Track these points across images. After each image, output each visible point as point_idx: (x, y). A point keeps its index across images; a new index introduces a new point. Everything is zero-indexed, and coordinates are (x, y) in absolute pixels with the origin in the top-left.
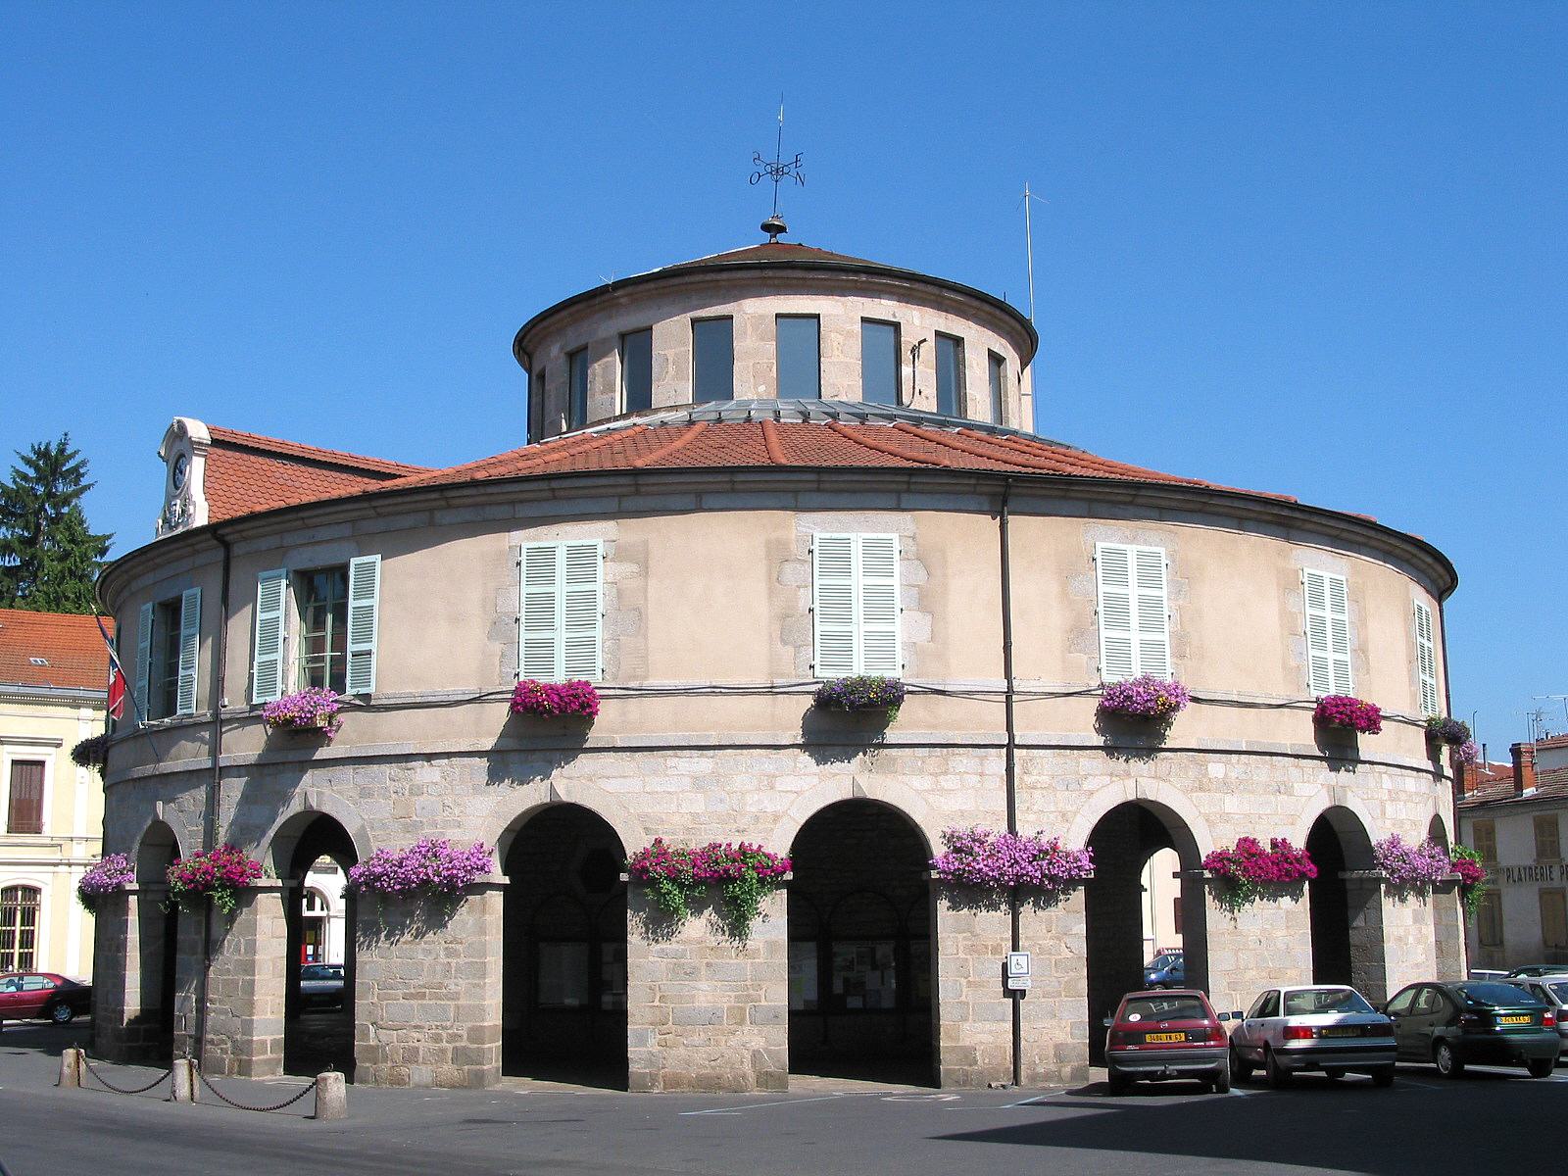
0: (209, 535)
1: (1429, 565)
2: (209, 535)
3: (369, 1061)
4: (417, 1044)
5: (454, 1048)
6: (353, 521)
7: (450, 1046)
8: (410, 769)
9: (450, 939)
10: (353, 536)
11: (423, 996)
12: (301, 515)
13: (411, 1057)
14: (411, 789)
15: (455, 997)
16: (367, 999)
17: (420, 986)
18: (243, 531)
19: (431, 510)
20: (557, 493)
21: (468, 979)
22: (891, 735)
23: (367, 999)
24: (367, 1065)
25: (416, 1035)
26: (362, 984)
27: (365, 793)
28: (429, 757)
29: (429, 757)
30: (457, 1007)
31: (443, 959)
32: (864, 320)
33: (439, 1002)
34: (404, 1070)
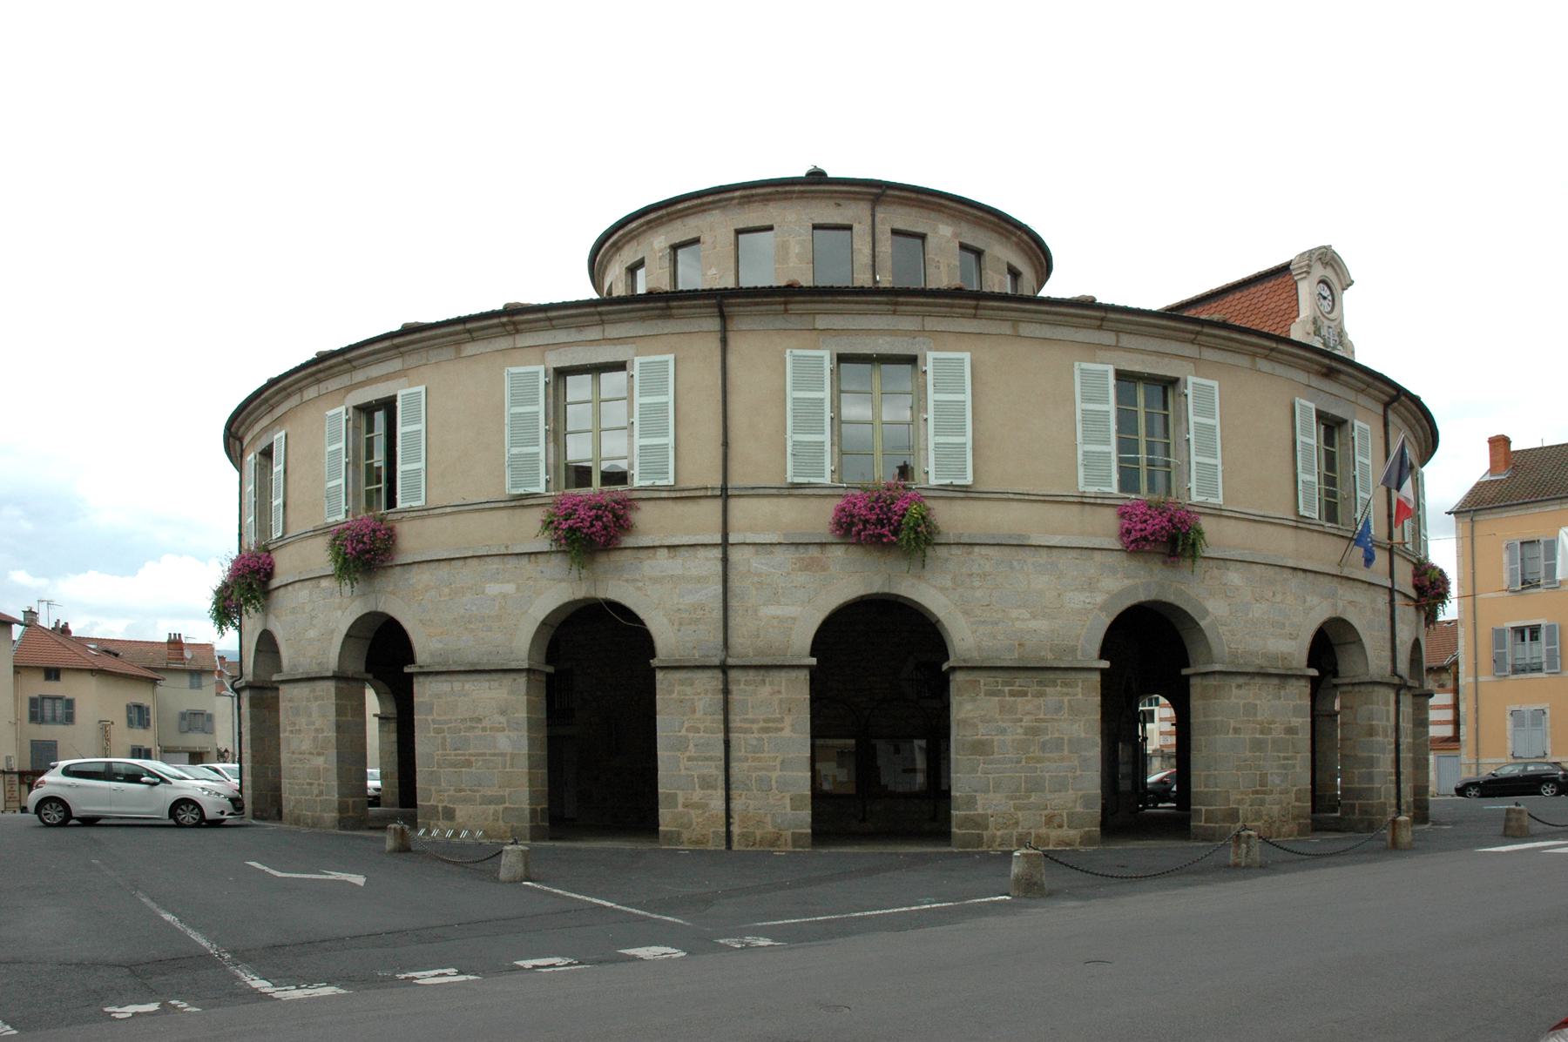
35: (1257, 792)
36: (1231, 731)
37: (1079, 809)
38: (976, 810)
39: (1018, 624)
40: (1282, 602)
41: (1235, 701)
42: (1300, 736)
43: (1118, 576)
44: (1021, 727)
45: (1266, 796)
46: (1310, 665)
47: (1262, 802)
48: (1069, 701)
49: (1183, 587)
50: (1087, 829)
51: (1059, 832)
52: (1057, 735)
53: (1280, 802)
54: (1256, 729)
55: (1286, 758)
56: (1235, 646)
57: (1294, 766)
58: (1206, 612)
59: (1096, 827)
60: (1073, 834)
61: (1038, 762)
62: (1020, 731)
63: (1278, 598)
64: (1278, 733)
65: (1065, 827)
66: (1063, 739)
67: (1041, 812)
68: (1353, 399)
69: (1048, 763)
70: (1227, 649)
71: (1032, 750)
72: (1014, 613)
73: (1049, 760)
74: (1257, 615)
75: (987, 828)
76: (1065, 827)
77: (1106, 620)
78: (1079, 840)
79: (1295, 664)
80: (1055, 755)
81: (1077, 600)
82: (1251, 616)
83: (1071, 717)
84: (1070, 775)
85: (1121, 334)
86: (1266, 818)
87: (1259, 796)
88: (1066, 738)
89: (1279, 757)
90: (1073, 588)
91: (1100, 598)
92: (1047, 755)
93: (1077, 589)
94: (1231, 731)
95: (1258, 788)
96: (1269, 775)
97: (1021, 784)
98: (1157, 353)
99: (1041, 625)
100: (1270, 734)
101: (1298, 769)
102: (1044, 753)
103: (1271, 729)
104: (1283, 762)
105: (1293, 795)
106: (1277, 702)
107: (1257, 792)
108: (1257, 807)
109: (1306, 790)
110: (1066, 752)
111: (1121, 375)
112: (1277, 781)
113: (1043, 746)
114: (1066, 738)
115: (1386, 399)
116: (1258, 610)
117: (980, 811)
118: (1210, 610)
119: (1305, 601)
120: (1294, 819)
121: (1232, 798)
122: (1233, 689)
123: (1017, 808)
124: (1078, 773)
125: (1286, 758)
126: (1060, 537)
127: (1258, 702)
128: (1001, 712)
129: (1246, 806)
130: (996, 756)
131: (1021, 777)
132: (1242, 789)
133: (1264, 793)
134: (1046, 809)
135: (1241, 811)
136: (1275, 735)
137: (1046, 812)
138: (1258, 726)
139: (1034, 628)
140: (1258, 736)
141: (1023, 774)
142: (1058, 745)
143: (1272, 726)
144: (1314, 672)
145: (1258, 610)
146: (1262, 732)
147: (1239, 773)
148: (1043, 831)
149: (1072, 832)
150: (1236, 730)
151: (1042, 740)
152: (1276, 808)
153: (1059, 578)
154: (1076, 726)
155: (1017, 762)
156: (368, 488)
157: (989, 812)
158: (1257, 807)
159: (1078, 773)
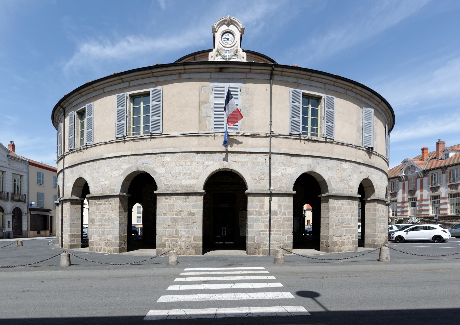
0: (70, 103)
1: (353, 87)
2: (70, 103)
3: (333, 246)
4: (344, 240)
5: (352, 241)
6: (347, 89)
7: (352, 240)
8: (341, 164)
9: (352, 212)
10: (324, 88)
11: (346, 227)
12: (80, 91)
13: (343, 244)
14: (342, 170)
15: (352, 227)
16: (332, 228)
17: (346, 224)
18: (82, 93)
19: (180, 74)
20: (124, 80)
21: (355, 222)
22: (375, 116)
23: (332, 228)
24: (333, 247)
25: (344, 238)
26: (331, 224)
27: (330, 169)
28: (346, 161)
29: (346, 161)
30: (353, 230)
31: (350, 217)
32: (13, 173)
33: (350, 229)
34: (342, 248)
35: (174, 237)
36: (163, 214)
37: (113, 241)
38: (92, 240)
39: (102, 183)
40: (190, 165)
41: (165, 204)
42: (196, 216)
43: (127, 164)
44: (100, 214)
45: (179, 239)
46: (359, 193)
47: (177, 241)
48: (111, 206)
49: (147, 165)
50: (115, 247)
51: (109, 248)
52: (108, 217)
53: (185, 242)
54: (174, 214)
55: (188, 225)
56: (167, 184)
57: (193, 228)
58: (156, 173)
59: (117, 247)
60: (111, 249)
61: (104, 225)
62: (100, 216)
63: (188, 164)
64: (184, 215)
65: (110, 247)
66: (109, 218)
67: (105, 241)
68: (244, 77)
69: (106, 226)
70: (163, 185)
71: (102, 222)
72: (101, 180)
73: (106, 225)
74: (177, 172)
75: (93, 246)
76: (110, 247)
77: (123, 179)
78: (113, 251)
79: (353, 193)
80: (107, 223)
81: (115, 173)
82: (174, 172)
83: (111, 211)
84: (111, 229)
85: (299, 79)
86: (178, 247)
87: (175, 239)
88: (110, 217)
89: (185, 224)
90: (115, 170)
91: (121, 172)
92: (106, 223)
93: (115, 170)
94: (163, 214)
95: (174, 235)
96: (180, 231)
97: (100, 233)
98: (142, 84)
99: (107, 182)
100: (181, 215)
101: (195, 229)
102: (105, 222)
103: (181, 214)
104: (186, 226)
105: (192, 239)
106: (185, 204)
107: (174, 237)
108: (174, 243)
109: (199, 237)
110: (110, 222)
111: (305, 95)
112: (184, 233)
113: (105, 220)
114: (110, 217)
115: (270, 72)
116: (177, 170)
117: (92, 240)
118: (157, 172)
119: (204, 163)
120: (193, 248)
121: (163, 239)
122: (164, 199)
123: (100, 240)
124: (113, 229)
125: (188, 225)
126: (111, 154)
127: (175, 204)
128: (97, 210)
129: (169, 242)
130: (96, 224)
131: (100, 230)
132: (167, 236)
133: (178, 237)
134: (106, 240)
135: (167, 244)
136: (182, 216)
137: (105, 241)
138: (174, 213)
139: (105, 183)
140: (175, 216)
141: (101, 229)
142: (108, 220)
143: (182, 212)
144: (360, 196)
145: (177, 170)
146: (177, 215)
147: (166, 230)
148: (105, 247)
149: (112, 248)
150: (165, 214)
151: (105, 218)
152: (183, 244)
153: (111, 167)
154: (112, 214)
155: (99, 226)
156: (440, 180)
157: (94, 241)
158: (174, 243)
159: (113, 229)
